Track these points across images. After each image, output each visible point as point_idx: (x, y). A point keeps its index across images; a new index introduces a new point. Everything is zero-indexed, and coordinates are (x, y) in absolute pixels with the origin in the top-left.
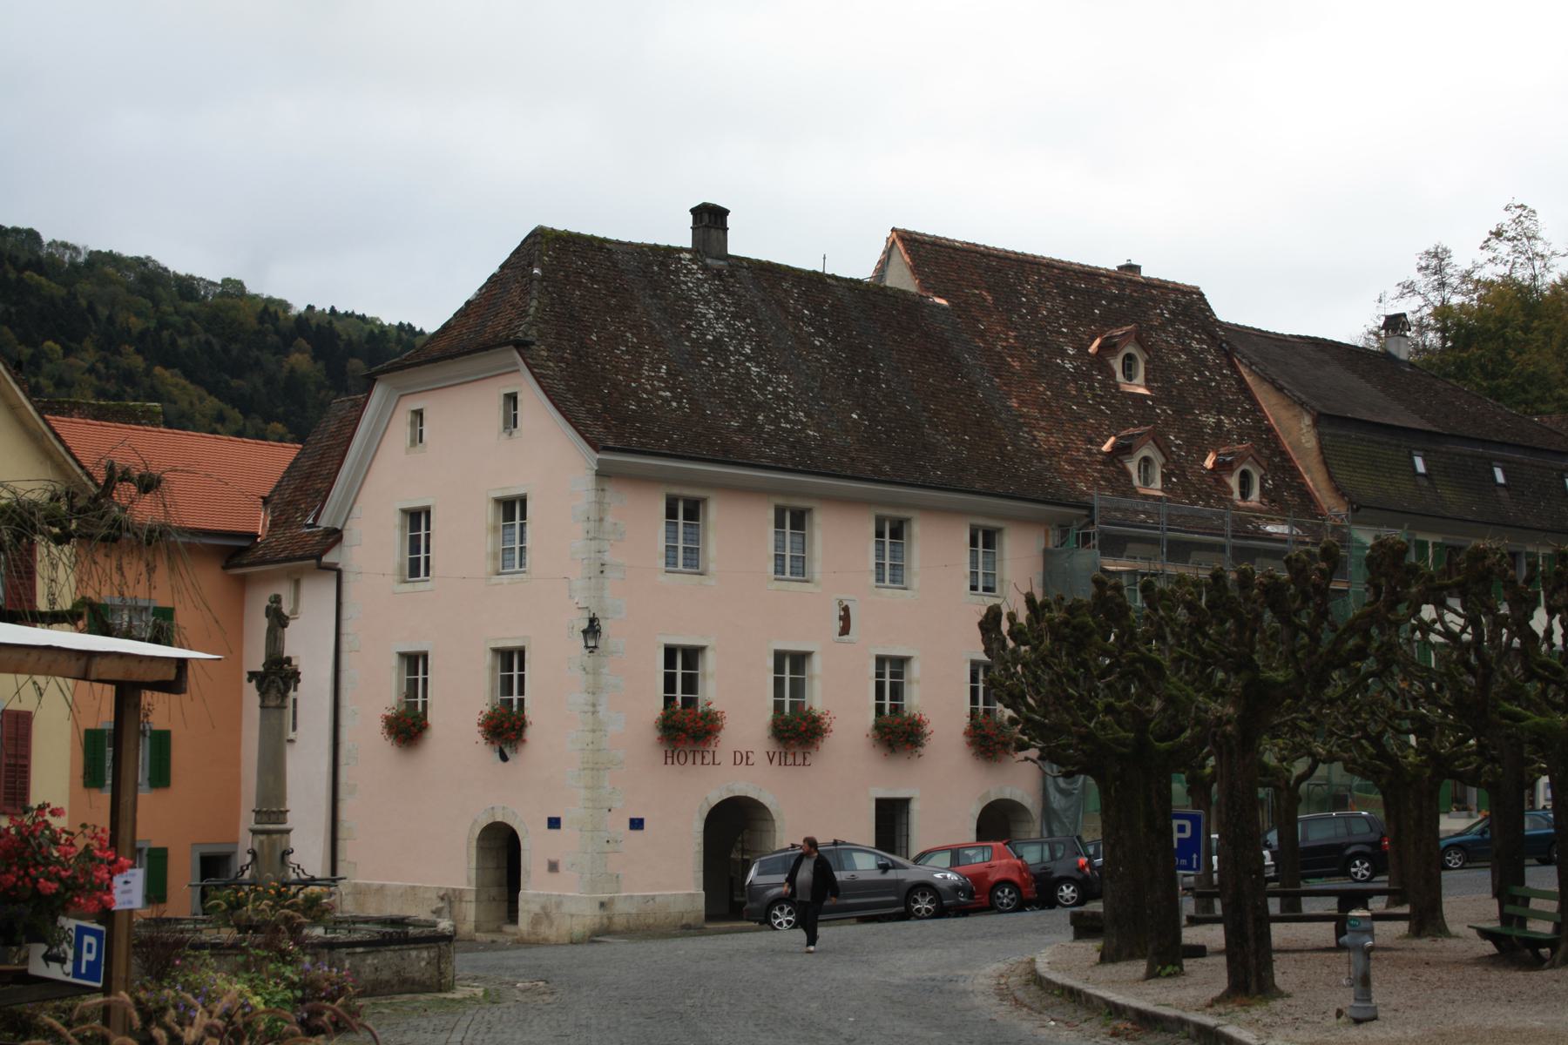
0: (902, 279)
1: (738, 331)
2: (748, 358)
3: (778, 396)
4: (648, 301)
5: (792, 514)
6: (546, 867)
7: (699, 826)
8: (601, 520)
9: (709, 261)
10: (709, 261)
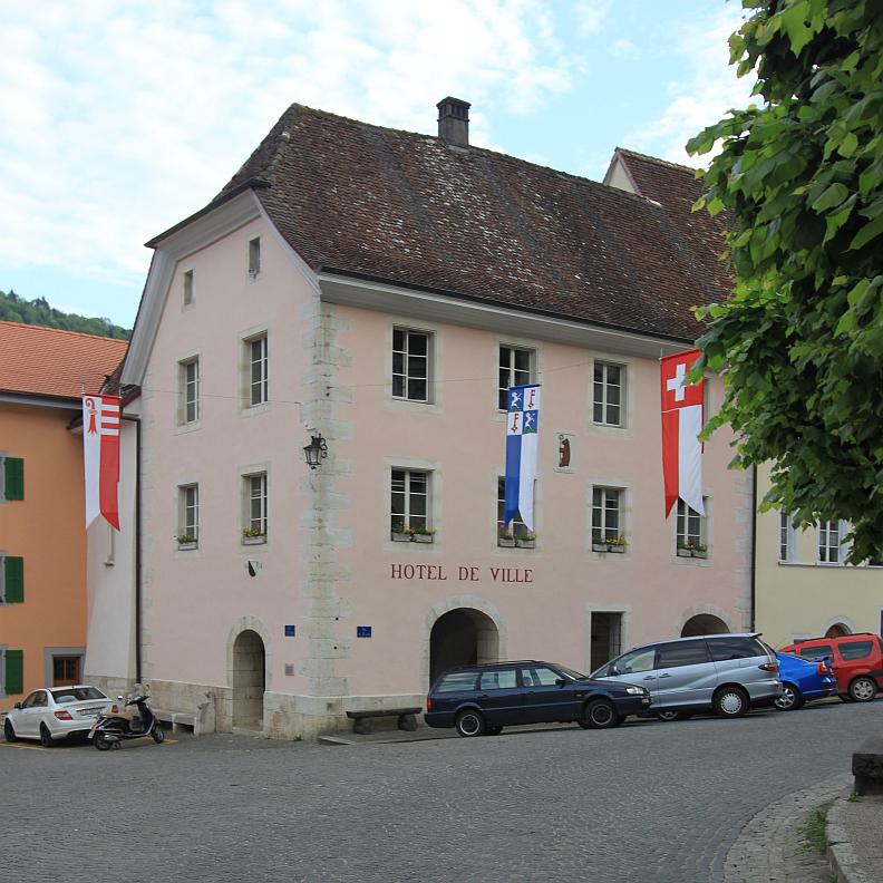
0: (623, 183)
1: (475, 202)
2: (482, 223)
3: (509, 255)
4: (392, 170)
5: (517, 353)
6: (284, 670)
7: (426, 635)
8: (327, 345)
9: (452, 148)
10: (452, 148)
